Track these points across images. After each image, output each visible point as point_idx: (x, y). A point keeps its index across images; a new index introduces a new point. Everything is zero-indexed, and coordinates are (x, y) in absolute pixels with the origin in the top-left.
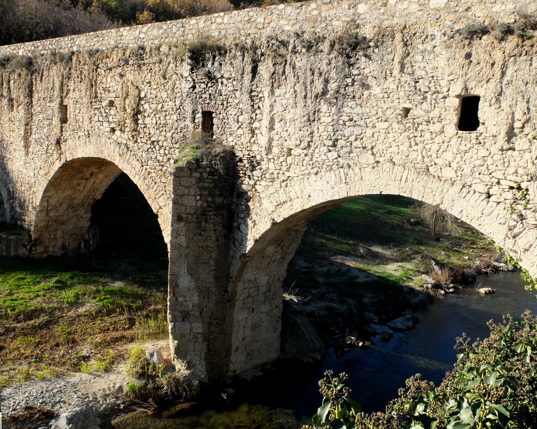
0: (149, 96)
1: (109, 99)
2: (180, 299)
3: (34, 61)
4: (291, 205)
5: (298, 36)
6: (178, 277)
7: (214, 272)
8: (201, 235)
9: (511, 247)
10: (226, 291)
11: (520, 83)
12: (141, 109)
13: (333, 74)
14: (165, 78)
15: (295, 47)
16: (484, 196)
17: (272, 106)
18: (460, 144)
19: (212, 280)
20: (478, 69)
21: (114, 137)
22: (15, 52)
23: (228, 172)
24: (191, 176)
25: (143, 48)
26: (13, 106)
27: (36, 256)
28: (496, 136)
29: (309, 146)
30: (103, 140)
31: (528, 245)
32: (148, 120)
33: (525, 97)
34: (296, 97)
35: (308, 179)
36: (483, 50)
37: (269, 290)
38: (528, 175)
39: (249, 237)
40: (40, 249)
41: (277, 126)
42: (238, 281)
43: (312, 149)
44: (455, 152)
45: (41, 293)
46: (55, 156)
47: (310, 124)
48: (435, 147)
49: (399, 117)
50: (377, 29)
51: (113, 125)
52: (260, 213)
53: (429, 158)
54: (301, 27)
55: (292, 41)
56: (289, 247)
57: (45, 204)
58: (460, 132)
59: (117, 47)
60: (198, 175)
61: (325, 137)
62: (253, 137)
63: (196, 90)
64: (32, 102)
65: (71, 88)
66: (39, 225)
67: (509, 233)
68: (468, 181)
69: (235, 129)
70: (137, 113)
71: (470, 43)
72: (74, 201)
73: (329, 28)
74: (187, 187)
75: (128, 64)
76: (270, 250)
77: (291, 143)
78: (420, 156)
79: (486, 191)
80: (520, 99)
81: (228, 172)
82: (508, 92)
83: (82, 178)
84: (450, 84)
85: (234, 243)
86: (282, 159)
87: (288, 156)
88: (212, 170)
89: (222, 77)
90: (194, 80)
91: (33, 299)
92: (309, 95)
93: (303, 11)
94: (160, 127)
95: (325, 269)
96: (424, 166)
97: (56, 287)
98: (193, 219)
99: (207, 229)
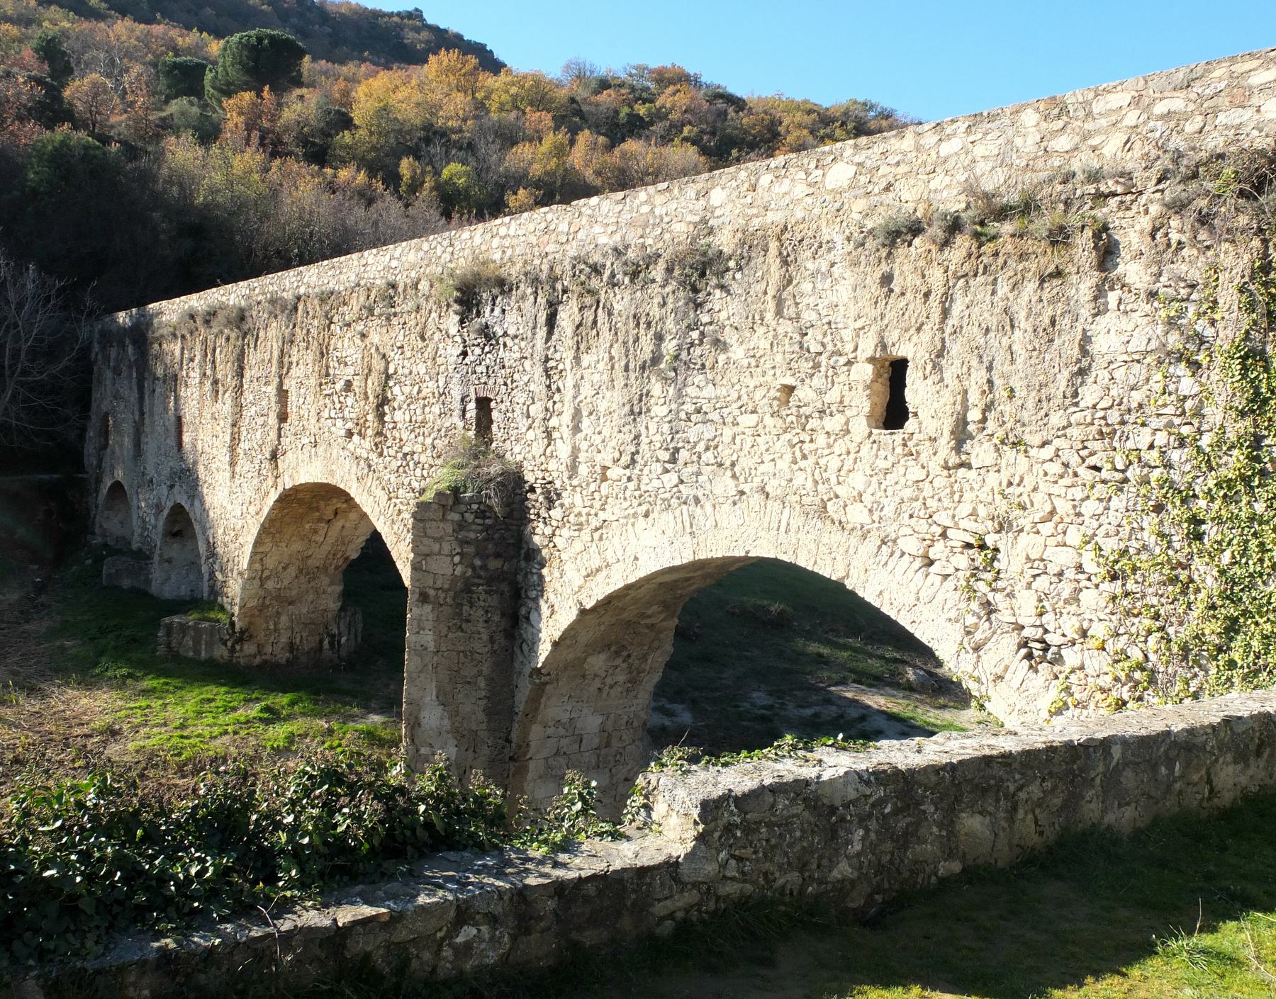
0: (400, 372)
1: (346, 378)
2: (423, 751)
3: (247, 314)
4: (608, 577)
5: (618, 252)
6: (419, 709)
7: (485, 701)
8: (462, 631)
9: (970, 669)
10: (508, 741)
11: (975, 329)
12: (389, 395)
13: (670, 324)
14: (423, 338)
15: (613, 275)
16: (918, 562)
17: (576, 386)
18: (877, 456)
19: (481, 716)
20: (901, 305)
21: (351, 446)
22: (224, 299)
23: (512, 511)
24: (444, 519)
25: (393, 286)
26: (217, 392)
27: (242, 661)
28: (935, 439)
29: (633, 461)
30: (335, 452)
31: (1002, 667)
32: (398, 416)
33: (985, 359)
34: (613, 368)
35: (633, 525)
36: (911, 267)
37: (608, 745)
38: (993, 519)
39: (543, 635)
40: (249, 648)
41: (586, 423)
42: (532, 722)
43: (638, 467)
44: (869, 472)
45: (230, 729)
46: (270, 481)
47: (634, 420)
48: (834, 463)
49: (775, 403)
50: (739, 235)
51: (350, 425)
52: (560, 589)
53: (826, 486)
54: (623, 238)
55: (608, 264)
56: (644, 658)
57: (258, 566)
58: (875, 431)
59: (358, 285)
60: (456, 517)
61: (658, 445)
62: (549, 444)
63: (467, 360)
64: (242, 386)
65: (294, 359)
66: (248, 605)
67: (966, 640)
68: (891, 530)
69: (524, 430)
70: (383, 401)
71: (890, 253)
72: (310, 562)
73: (667, 236)
74: (436, 540)
75: (373, 315)
76: (598, 662)
77: (606, 458)
78: (810, 479)
79: (921, 552)
80: (975, 362)
81: (512, 511)
82: (956, 348)
83: (320, 520)
84: (858, 336)
85: (521, 647)
86: (593, 487)
87: (602, 481)
88: (482, 507)
89: (505, 334)
90: (465, 341)
91: (216, 737)
92: (631, 366)
93: (628, 207)
94: (417, 426)
95: (808, 712)
96: (817, 500)
97: (260, 719)
98: (448, 600)
99: (472, 618)
